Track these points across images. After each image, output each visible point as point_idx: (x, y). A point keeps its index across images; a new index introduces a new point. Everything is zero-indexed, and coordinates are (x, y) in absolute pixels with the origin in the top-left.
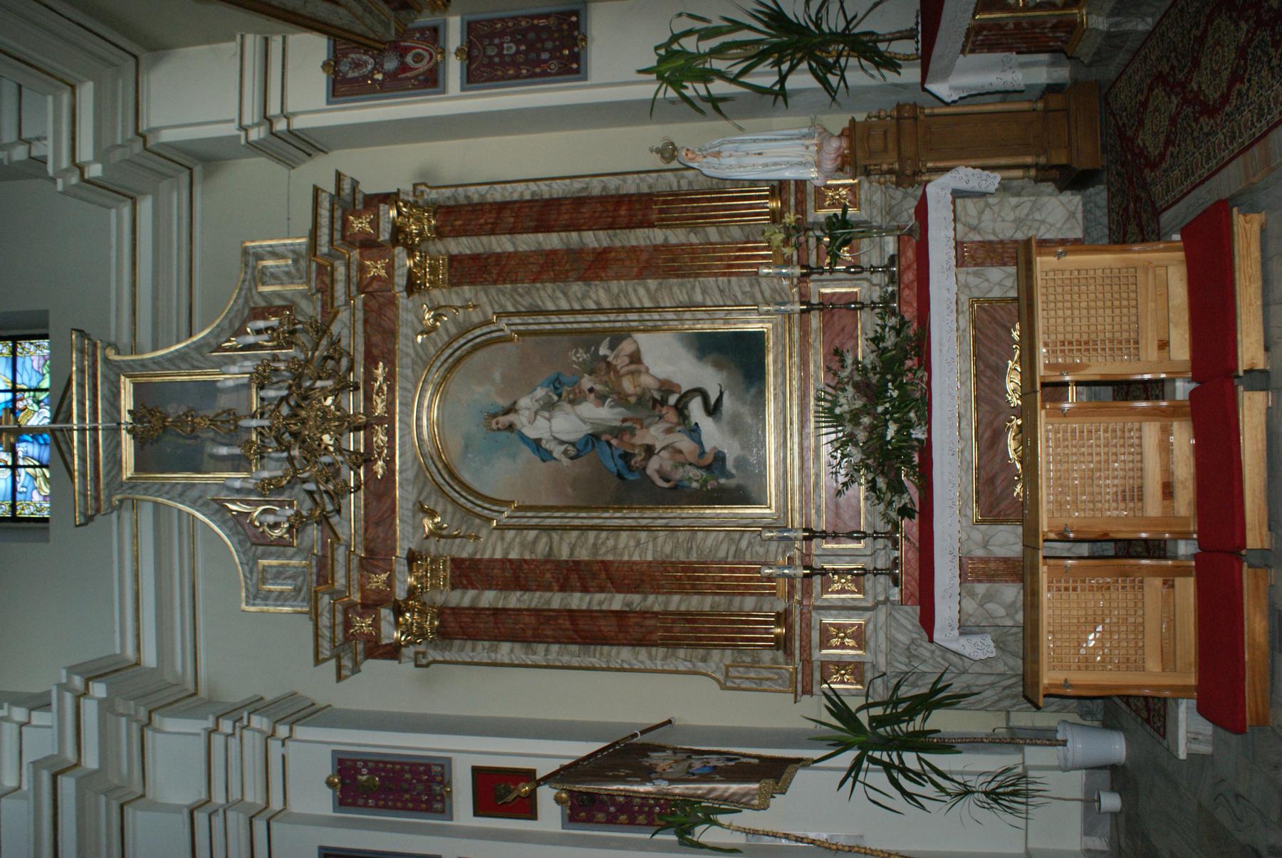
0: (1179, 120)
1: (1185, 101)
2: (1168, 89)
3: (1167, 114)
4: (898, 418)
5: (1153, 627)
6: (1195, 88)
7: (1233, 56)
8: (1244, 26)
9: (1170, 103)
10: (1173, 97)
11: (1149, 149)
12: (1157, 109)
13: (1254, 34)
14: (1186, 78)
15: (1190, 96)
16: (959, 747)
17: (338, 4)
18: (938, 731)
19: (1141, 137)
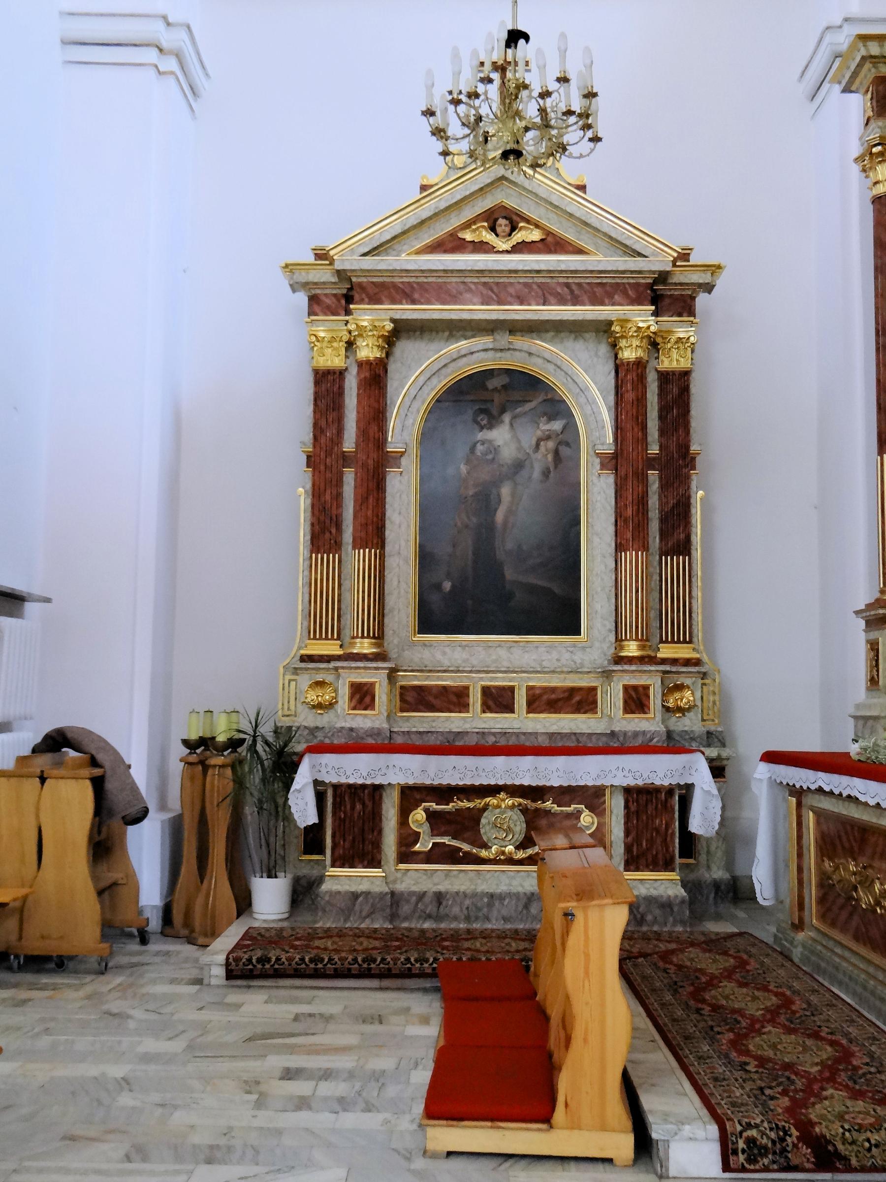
0: (857, 1087)
1: (832, 1080)
2: (812, 1100)
3: (849, 1103)
4: (482, 899)
5: (458, 280)
6: (760, 1012)
7: (861, 1103)
8: (830, 1091)
9: (832, 1097)
10: (824, 1093)
11: (825, 1057)
12: (774, 1047)
13: (840, 1084)
14: (802, 1077)
15: (769, 1016)
16: (97, 819)
17: (881, 453)
18: (170, 1039)
19: (836, 1093)
